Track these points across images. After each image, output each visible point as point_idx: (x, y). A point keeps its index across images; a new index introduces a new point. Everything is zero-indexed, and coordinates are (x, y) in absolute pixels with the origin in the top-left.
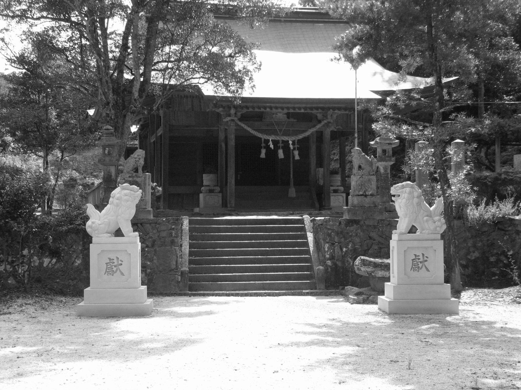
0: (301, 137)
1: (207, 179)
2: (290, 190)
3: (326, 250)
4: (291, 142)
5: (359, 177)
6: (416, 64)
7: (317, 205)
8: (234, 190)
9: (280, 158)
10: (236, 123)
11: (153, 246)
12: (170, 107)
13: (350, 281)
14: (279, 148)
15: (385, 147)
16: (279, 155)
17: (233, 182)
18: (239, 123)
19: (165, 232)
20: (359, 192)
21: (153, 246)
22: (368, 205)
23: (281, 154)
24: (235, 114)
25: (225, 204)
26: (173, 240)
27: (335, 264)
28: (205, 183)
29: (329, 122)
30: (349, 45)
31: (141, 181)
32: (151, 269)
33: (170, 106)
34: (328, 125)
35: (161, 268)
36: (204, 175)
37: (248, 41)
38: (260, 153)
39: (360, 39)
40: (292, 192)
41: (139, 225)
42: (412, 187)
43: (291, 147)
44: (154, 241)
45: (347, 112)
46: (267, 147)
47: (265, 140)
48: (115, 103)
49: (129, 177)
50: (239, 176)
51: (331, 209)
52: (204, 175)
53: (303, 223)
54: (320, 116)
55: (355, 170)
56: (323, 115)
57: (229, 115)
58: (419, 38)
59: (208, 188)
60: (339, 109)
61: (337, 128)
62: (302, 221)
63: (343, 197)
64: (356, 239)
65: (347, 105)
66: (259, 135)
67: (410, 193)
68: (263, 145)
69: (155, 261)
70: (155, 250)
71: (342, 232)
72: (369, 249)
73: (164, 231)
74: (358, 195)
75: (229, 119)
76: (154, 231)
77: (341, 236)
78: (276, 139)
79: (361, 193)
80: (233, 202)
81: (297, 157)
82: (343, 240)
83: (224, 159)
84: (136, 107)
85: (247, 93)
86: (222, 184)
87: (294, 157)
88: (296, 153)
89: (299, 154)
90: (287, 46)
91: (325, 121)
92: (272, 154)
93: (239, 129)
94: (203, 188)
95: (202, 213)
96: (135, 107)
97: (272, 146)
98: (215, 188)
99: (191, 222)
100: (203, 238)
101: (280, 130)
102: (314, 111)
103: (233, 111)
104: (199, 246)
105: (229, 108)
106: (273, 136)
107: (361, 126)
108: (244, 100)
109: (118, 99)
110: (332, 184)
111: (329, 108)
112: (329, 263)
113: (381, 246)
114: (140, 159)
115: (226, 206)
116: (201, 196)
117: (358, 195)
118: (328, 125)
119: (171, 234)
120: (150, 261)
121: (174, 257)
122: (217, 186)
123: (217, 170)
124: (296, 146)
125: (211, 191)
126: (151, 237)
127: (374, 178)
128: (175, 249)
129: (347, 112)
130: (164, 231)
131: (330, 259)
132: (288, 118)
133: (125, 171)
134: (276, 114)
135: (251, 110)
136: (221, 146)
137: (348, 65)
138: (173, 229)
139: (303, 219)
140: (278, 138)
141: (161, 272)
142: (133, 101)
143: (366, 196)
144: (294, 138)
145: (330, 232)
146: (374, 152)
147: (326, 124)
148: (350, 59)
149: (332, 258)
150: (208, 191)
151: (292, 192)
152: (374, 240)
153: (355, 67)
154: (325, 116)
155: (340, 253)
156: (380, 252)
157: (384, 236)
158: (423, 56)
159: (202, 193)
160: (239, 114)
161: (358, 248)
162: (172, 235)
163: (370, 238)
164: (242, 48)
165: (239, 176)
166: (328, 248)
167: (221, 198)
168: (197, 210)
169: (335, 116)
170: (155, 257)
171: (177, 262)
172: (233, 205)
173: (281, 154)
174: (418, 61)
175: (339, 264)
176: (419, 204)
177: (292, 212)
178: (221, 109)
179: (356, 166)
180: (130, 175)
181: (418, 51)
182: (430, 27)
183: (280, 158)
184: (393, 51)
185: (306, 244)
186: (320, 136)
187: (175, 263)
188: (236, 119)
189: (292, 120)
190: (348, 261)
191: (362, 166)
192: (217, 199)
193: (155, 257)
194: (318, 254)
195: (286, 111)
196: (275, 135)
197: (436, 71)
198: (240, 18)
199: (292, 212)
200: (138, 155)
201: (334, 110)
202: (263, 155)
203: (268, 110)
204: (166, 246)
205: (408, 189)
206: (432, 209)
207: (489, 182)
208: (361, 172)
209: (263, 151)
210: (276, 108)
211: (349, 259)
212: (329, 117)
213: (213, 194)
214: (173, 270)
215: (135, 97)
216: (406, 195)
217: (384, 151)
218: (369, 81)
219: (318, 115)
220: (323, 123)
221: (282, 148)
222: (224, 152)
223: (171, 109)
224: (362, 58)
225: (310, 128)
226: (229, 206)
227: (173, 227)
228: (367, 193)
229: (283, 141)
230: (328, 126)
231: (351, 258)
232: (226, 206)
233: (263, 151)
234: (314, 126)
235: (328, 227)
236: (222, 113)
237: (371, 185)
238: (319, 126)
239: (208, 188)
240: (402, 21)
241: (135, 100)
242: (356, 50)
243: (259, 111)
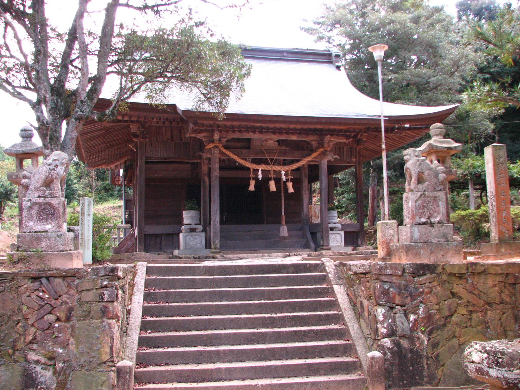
0: (295, 166)
1: (188, 217)
2: (281, 228)
3: (381, 318)
4: (283, 173)
5: (419, 194)
7: (313, 245)
8: (218, 229)
9: (271, 191)
10: (220, 150)
11: (68, 319)
12: (146, 138)
13: (425, 374)
16: (271, 188)
17: (218, 219)
19: (91, 292)
20: (420, 218)
21: (68, 319)
22: (437, 240)
23: (273, 187)
24: (220, 140)
25: (208, 245)
26: (106, 307)
27: (397, 344)
28: (185, 221)
31: (59, 204)
32: (64, 362)
33: (147, 136)
34: (324, 154)
35: (82, 360)
36: (184, 212)
38: (249, 185)
40: (284, 231)
41: (44, 280)
43: (284, 178)
44: (71, 310)
46: (256, 179)
47: (254, 169)
48: (54, 106)
49: (39, 197)
50: (224, 217)
51: (330, 249)
52: (184, 212)
53: (324, 270)
54: (314, 144)
56: (318, 144)
57: (213, 142)
59: (189, 227)
61: (334, 157)
62: (320, 267)
63: (341, 235)
64: (432, 298)
68: (252, 176)
69: (71, 347)
70: (72, 327)
71: (406, 287)
72: (452, 315)
73: (88, 290)
74: (420, 224)
75: (211, 146)
76: (72, 292)
77: (406, 293)
78: (266, 169)
79: (423, 220)
80: (218, 242)
81: (291, 190)
82: (408, 300)
83: (207, 194)
84: (83, 112)
85: (237, 104)
86: (205, 222)
87: (286, 189)
88: (290, 185)
89: (293, 187)
91: (322, 150)
92: (262, 185)
93: (227, 165)
94: (183, 227)
95: (181, 256)
96: (81, 111)
98: (197, 226)
99: (149, 271)
100: (167, 298)
103: (216, 136)
104: (160, 312)
106: (263, 165)
109: (59, 101)
110: (330, 221)
112: (387, 342)
113: (471, 309)
114: (57, 166)
115: (210, 248)
116: (181, 235)
117: (420, 224)
119: (102, 295)
120: (64, 347)
121: (108, 339)
122: (200, 224)
123: (200, 206)
124: (290, 177)
125: (193, 230)
126: (66, 303)
128: (109, 325)
130: (88, 290)
131: (388, 336)
132: (279, 145)
133: (32, 187)
134: (266, 141)
136: (204, 181)
138: (106, 287)
139: (323, 264)
140: (269, 168)
141: (82, 366)
142: (79, 103)
143: (432, 224)
144: (287, 168)
145: (386, 287)
147: (322, 152)
149: (392, 333)
150: (189, 231)
151: (284, 231)
152: (460, 298)
154: (321, 144)
155: (406, 324)
156: (470, 319)
157: (476, 292)
159: (182, 232)
160: (224, 140)
161: (435, 314)
162: (103, 299)
163: (453, 294)
165: (224, 217)
166: (384, 316)
167: (203, 239)
168: (176, 252)
169: (331, 144)
170: (72, 340)
171: (111, 348)
172: (218, 246)
173: (273, 187)
175: (405, 343)
177: (288, 254)
180: (41, 193)
183: (271, 191)
185: (334, 304)
187: (108, 350)
189: (284, 148)
190: (418, 338)
192: (199, 239)
193: (72, 340)
194: (359, 322)
196: (265, 164)
199: (288, 254)
200: (54, 160)
202: (252, 188)
204: (92, 318)
207: (476, 219)
209: (252, 183)
211: (420, 333)
212: (326, 145)
213: (194, 233)
214: (105, 363)
215: (82, 99)
219: (313, 143)
221: (274, 179)
222: (208, 187)
223: (147, 140)
225: (305, 157)
226: (213, 247)
227: (105, 283)
228: (432, 220)
229: (274, 171)
231: (423, 332)
232: (210, 248)
233: (252, 183)
234: (309, 155)
235: (384, 278)
236: (204, 140)
237: (438, 206)
238: (314, 155)
239: (189, 227)
241: (82, 102)
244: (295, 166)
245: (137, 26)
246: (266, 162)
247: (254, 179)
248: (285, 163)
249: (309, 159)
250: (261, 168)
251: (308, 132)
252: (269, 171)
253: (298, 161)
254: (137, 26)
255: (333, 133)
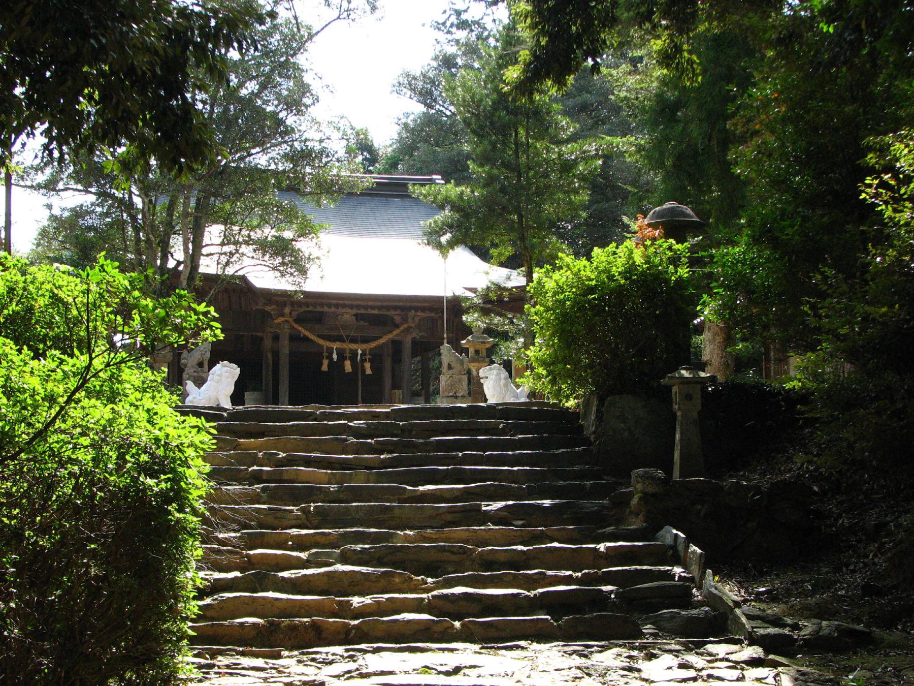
0: (373, 345)
4: (360, 352)
6: (507, 254)
14: (345, 359)
15: (478, 347)
18: (296, 326)
29: (410, 327)
30: (439, 232)
37: (316, 223)
38: (321, 364)
39: (450, 227)
42: (499, 369)
45: (433, 315)
54: (398, 319)
55: (444, 369)
57: (283, 315)
58: (511, 228)
60: (423, 309)
65: (430, 306)
66: (321, 342)
67: (498, 374)
68: (325, 354)
75: (281, 319)
79: (451, 394)
81: (369, 371)
87: (364, 370)
88: (367, 365)
90: (350, 225)
91: (405, 326)
93: (295, 338)
97: (335, 356)
101: (348, 336)
102: (391, 313)
103: (287, 310)
105: (284, 305)
107: (451, 335)
108: (307, 294)
111: (410, 308)
118: (408, 330)
127: (465, 378)
129: (433, 315)
132: (357, 319)
133: (189, 365)
135: (311, 308)
137: (437, 252)
144: (365, 346)
146: (466, 351)
148: (439, 246)
153: (445, 255)
154: (405, 320)
158: (514, 244)
160: (295, 314)
164: (306, 230)
169: (417, 319)
174: (509, 251)
176: (506, 385)
178: (274, 307)
179: (445, 365)
181: (510, 240)
182: (520, 217)
184: (483, 239)
186: (397, 345)
188: (291, 320)
189: (362, 323)
191: (453, 365)
195: (355, 311)
197: (527, 261)
198: (304, 195)
201: (416, 311)
202: (325, 368)
203: (333, 309)
205: (495, 372)
206: (518, 391)
208: (451, 372)
209: (326, 362)
210: (344, 306)
212: (410, 320)
216: (494, 377)
217: (477, 352)
218: (462, 274)
219: (396, 317)
220: (402, 328)
221: (350, 359)
224: (452, 244)
229: (351, 349)
230: (407, 334)
233: (326, 362)
234: (391, 332)
240: (491, 210)
242: (444, 239)
243: (318, 309)
244: (373, 345)
245: (670, 668)
246: (340, 339)
247: (327, 358)
248: (365, 340)
249: (390, 336)
250: (335, 346)
251: (388, 308)
252: (344, 350)
253: (375, 339)
254: (670, 668)
255: (416, 309)
